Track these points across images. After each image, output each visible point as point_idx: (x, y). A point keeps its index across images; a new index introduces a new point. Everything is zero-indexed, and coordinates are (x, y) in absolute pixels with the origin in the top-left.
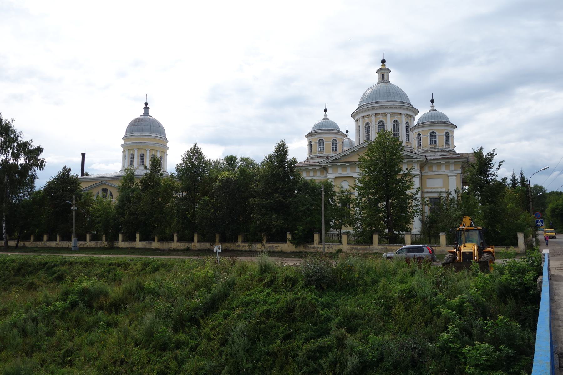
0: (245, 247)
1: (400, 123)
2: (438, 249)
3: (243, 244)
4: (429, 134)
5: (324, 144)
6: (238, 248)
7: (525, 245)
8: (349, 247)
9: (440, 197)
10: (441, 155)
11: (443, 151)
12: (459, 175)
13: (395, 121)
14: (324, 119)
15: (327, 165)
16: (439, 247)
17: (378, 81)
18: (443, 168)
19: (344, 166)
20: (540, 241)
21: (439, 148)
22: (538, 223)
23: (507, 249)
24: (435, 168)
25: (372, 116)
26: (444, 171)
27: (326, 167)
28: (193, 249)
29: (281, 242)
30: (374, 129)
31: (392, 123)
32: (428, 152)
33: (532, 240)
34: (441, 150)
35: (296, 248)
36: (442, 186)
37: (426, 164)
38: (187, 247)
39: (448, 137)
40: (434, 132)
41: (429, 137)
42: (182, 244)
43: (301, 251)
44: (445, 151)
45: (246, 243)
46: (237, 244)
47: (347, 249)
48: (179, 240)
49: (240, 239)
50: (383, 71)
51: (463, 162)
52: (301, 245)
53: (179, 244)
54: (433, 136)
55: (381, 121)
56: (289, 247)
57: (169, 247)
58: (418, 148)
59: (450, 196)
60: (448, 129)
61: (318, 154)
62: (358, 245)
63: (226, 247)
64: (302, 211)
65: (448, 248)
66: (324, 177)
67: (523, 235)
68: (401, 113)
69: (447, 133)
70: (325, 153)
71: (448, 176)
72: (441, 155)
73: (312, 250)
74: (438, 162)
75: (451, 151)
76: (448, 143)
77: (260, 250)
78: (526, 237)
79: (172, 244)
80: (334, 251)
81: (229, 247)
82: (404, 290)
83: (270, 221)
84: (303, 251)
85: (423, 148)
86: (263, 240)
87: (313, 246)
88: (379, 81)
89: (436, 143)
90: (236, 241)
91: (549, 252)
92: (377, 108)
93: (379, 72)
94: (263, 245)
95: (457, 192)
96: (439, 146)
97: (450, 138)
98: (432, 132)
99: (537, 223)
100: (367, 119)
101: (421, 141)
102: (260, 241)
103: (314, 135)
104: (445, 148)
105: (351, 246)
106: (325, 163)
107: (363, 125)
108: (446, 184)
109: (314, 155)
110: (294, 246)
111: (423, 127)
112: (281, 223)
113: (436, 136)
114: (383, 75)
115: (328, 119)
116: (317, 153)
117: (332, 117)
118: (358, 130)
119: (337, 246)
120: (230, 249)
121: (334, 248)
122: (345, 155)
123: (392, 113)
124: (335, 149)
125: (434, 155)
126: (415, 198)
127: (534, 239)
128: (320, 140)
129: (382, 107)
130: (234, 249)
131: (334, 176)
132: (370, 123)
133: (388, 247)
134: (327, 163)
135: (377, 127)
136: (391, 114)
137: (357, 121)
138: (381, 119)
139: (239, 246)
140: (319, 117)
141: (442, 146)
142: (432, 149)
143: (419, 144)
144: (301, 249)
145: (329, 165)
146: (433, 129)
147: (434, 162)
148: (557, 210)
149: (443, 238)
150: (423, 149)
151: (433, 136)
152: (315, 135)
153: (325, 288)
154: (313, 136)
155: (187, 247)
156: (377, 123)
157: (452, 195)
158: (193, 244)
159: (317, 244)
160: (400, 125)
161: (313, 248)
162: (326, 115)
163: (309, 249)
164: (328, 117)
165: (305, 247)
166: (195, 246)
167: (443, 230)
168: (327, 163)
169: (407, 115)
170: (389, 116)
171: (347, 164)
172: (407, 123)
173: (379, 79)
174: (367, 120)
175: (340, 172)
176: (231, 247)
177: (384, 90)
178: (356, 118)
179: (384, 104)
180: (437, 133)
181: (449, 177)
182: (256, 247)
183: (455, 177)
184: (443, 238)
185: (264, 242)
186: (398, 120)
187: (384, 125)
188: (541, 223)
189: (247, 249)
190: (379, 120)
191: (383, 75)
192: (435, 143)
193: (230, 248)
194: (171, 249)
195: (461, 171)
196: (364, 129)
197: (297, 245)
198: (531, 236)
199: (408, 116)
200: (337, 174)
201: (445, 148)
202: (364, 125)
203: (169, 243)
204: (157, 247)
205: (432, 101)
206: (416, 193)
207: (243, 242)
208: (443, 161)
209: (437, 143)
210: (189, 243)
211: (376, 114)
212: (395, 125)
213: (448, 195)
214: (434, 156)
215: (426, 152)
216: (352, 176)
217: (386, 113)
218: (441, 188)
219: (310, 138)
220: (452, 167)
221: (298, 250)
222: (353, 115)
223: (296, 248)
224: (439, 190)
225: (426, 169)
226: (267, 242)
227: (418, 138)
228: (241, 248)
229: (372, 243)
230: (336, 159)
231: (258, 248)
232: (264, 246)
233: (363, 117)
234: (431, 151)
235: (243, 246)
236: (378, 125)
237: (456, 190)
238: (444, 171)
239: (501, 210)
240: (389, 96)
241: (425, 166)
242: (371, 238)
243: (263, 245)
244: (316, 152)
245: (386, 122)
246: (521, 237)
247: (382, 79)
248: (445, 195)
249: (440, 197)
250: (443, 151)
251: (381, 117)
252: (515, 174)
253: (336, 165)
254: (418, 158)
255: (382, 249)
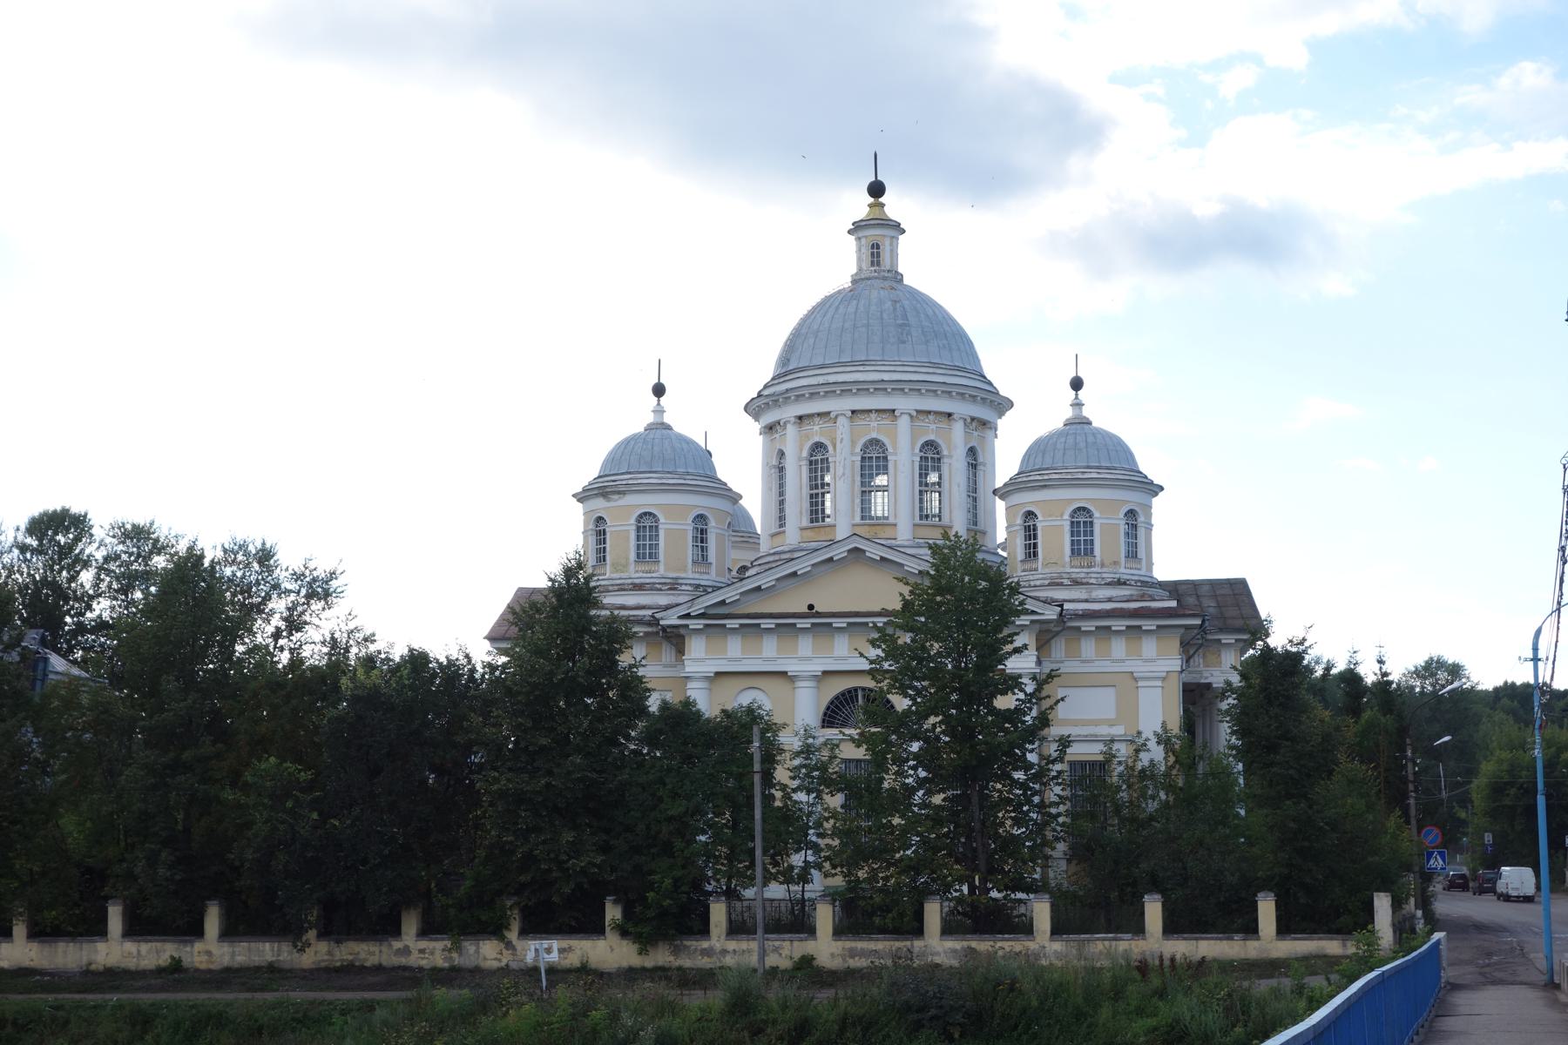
0: (432, 953)
1: (945, 452)
2: (1137, 946)
3: (423, 944)
4: (1066, 516)
5: (662, 533)
6: (403, 961)
7: (1394, 932)
8: (839, 946)
9: (1110, 757)
10: (1110, 600)
11: (1120, 583)
12: (1176, 674)
13: (930, 445)
14: (650, 428)
15: (687, 626)
16: (1141, 943)
17: (854, 270)
18: (1118, 647)
19: (752, 627)
20: (1438, 920)
21: (1105, 570)
22: (1432, 862)
23: (1344, 946)
24: (1088, 647)
25: (841, 420)
26: (1123, 661)
27: (682, 631)
28: (197, 965)
29: (159, 934)
30: (848, 472)
31: (917, 451)
32: (1061, 584)
33: (1413, 916)
34: (1109, 577)
35: (640, 954)
36: (1112, 715)
37: (1057, 633)
38: (172, 958)
39: (1135, 524)
40: (1084, 509)
41: (1067, 528)
42: (145, 947)
43: (660, 963)
44: (1125, 584)
45: (436, 940)
46: (397, 945)
47: (832, 955)
48: (135, 929)
49: (410, 925)
50: (878, 232)
51: (1187, 627)
52: (661, 944)
53: (130, 946)
54: (1082, 522)
55: (875, 442)
56: (612, 950)
57: (85, 960)
58: (1027, 566)
59: (1142, 755)
60: (1133, 498)
61: (635, 573)
62: (871, 939)
63: (350, 958)
64: (670, 819)
65: (1170, 943)
66: (660, 668)
67: (1390, 898)
68: (950, 415)
69: (1131, 514)
70: (662, 571)
71: (1136, 680)
72: (1110, 600)
73: (704, 962)
74: (1102, 622)
75: (1144, 583)
76: (1132, 554)
77: (495, 964)
78: (1397, 904)
79: (101, 946)
80: (785, 964)
81: (362, 956)
82: (1155, 1029)
83: (552, 855)
84: (667, 965)
85: (1043, 567)
86: (508, 928)
87: (705, 944)
88: (860, 269)
89: (1092, 550)
90: (396, 932)
91: (740, 502)
92: (862, 389)
93: (861, 234)
94: (509, 945)
95: (1164, 740)
96: (1103, 565)
97: (1141, 532)
98: (1079, 509)
99: (1428, 862)
100: (816, 428)
101: (1040, 541)
102: (495, 930)
103: (619, 493)
104: (1124, 571)
105: (849, 944)
106: (680, 617)
107: (801, 450)
108: (1127, 708)
109: (615, 576)
110: (636, 946)
111: (1045, 486)
112: (595, 865)
113: (1091, 523)
114: (875, 246)
115: (669, 428)
116: (632, 567)
117: (685, 420)
118: (777, 469)
119: (796, 944)
120: (368, 964)
121: (785, 952)
122: (758, 589)
123: (918, 412)
124: (702, 558)
125: (1084, 596)
126: (1054, 773)
127: (1419, 913)
128: (641, 516)
129: (880, 388)
130: (385, 963)
131: (711, 668)
132: (830, 448)
133: (974, 944)
134: (687, 616)
135: (858, 464)
136: (911, 417)
137: (770, 429)
138: (874, 435)
139: (406, 951)
140: (635, 418)
141: (1116, 563)
142: (1078, 572)
143: (1031, 552)
144: (661, 957)
145: (695, 624)
146: (1081, 496)
147: (1088, 626)
148: (1513, 791)
149: (1153, 910)
150: (1047, 571)
151: (1082, 522)
152: (623, 493)
153: (956, 1036)
154: (616, 497)
155: (172, 958)
156: (858, 450)
157: (1148, 750)
158: (198, 946)
159: (723, 937)
160: (945, 460)
161: (707, 953)
162: (659, 411)
163: (694, 956)
164: (667, 419)
165: (676, 951)
166: (209, 953)
167: (1155, 885)
168: (687, 616)
169: (973, 419)
170: (904, 423)
171: (767, 623)
172: (972, 451)
173: (859, 260)
174: (817, 432)
175: (735, 653)
176: (373, 954)
177: (885, 316)
178: (770, 418)
179: (886, 377)
180: (1097, 514)
181: (1140, 684)
182: (477, 952)
183: (1159, 683)
184: (1153, 910)
185: (513, 935)
186: (940, 441)
187: (885, 458)
188: (1441, 862)
189: (440, 961)
190: (868, 437)
191: (875, 246)
192: (1090, 552)
193: (366, 960)
194: (93, 967)
195: (1179, 662)
196: (805, 470)
197: (645, 942)
198: (1412, 900)
199: (974, 424)
200: (724, 662)
201: (1122, 570)
202: (805, 453)
203: (85, 946)
204: (26, 963)
205: (1077, 384)
206: (1055, 755)
207: (425, 932)
208: (1119, 624)
209: (1097, 551)
210: (181, 941)
211: (853, 412)
212: (927, 458)
213: (1137, 751)
214: (1086, 601)
215: (1055, 584)
216: (785, 673)
217: (894, 411)
218: (1111, 724)
219: (599, 504)
220: (1149, 647)
221: (649, 962)
222: (755, 408)
223: (640, 954)
224: (1104, 731)
225: (1059, 648)
226: (525, 932)
227: (1027, 529)
228: (414, 960)
229: (919, 931)
230: (723, 603)
231: (485, 959)
232: (514, 948)
233: (800, 418)
234: (1076, 583)
235: (422, 951)
236: (863, 459)
237: (1159, 731)
238: (1123, 661)
239: (1327, 824)
240: (904, 342)
241: (1053, 641)
242: (919, 916)
243: (509, 945)
244: (626, 566)
245: (895, 448)
246: (1382, 904)
247: (872, 264)
248: (1123, 750)
249: (1110, 757)
250: (1120, 583)
251: (874, 424)
252: (1359, 657)
253: (724, 625)
254: (1033, 612)
255: (954, 951)
